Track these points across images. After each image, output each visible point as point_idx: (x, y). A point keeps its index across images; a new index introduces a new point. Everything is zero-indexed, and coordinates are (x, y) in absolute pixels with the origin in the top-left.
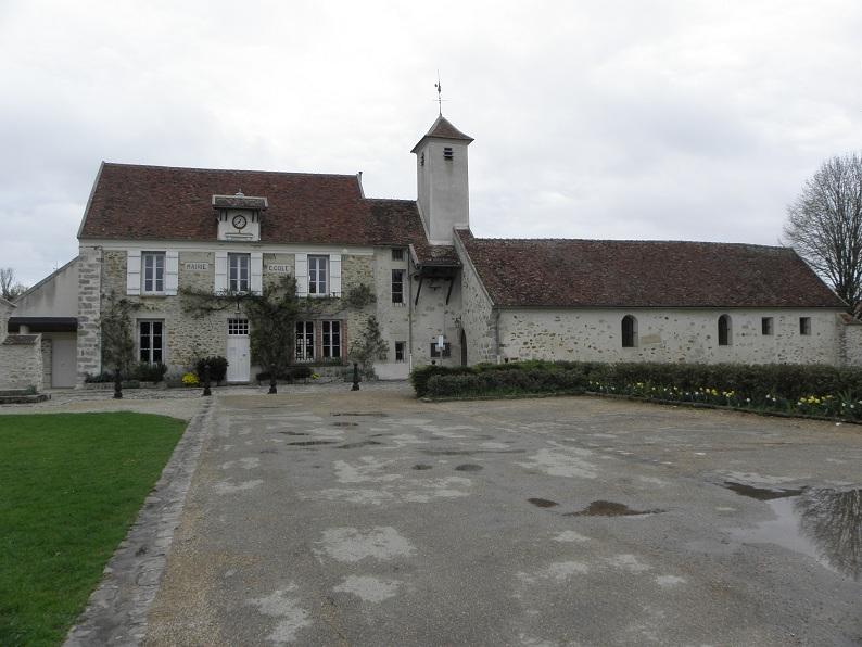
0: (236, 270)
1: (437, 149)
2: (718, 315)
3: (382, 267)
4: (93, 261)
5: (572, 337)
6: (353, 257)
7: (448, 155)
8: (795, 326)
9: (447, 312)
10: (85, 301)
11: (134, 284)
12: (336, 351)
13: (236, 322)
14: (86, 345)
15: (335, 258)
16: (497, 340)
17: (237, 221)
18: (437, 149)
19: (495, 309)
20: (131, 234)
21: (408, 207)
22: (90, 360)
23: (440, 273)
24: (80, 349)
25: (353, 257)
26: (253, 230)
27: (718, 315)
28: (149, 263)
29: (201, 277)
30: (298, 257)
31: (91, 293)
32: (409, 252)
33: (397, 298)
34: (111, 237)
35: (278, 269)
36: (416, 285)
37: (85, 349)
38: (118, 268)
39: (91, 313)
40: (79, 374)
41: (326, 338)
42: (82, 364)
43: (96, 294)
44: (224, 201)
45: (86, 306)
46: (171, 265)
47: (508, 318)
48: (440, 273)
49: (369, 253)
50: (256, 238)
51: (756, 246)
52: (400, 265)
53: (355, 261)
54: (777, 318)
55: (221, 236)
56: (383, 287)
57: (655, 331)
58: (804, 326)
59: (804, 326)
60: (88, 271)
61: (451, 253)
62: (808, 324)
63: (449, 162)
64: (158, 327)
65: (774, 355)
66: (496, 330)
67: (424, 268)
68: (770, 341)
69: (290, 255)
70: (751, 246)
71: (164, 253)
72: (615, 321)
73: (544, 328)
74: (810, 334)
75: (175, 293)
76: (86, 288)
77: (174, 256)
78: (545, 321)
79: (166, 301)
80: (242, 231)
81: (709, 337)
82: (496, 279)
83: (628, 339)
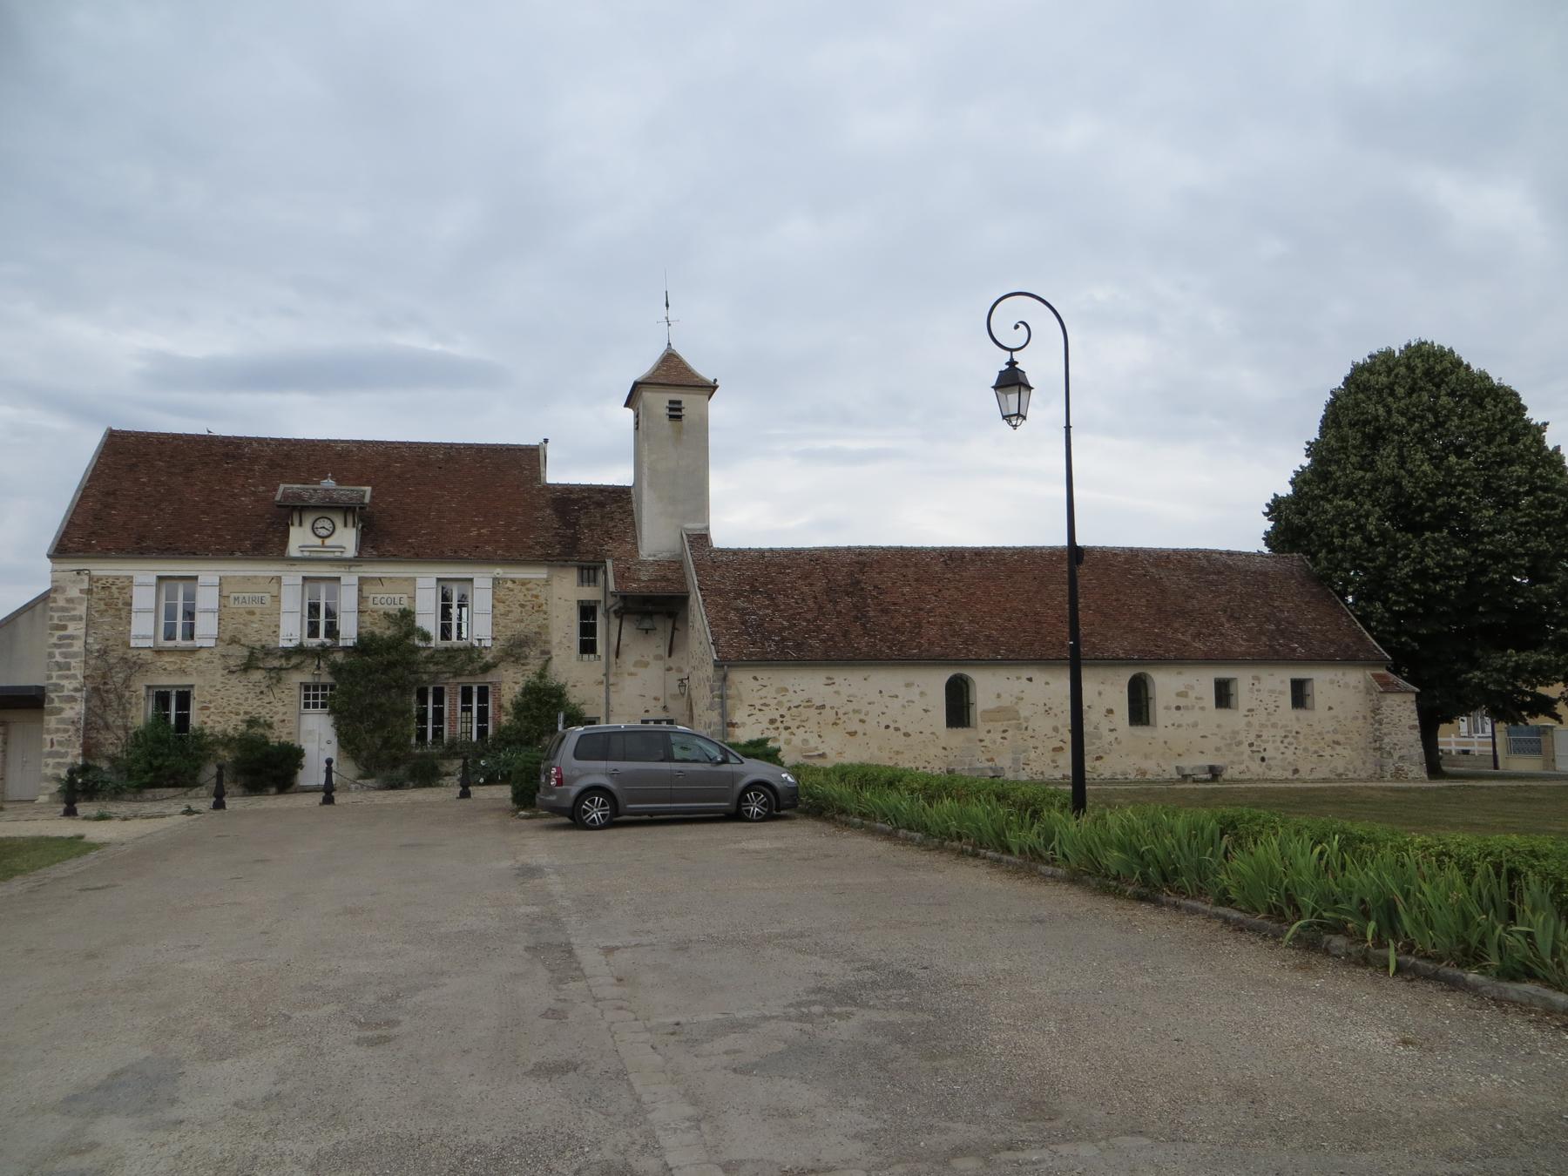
0: (175, 606)
1: (658, 401)
2: (1124, 676)
3: (564, 592)
4: (74, 592)
5: (855, 711)
6: (514, 581)
7: (675, 412)
8: (1281, 693)
9: (669, 669)
10: (58, 658)
11: (143, 628)
12: (438, 733)
13: (316, 688)
14: (57, 730)
15: (482, 582)
16: (723, 715)
17: (319, 524)
18: (658, 401)
19: (718, 665)
20: (141, 547)
21: (619, 496)
22: (65, 755)
23: (655, 607)
24: (48, 737)
25: (514, 581)
26: (346, 538)
27: (1124, 676)
28: (171, 596)
29: (256, 618)
30: (420, 583)
31: (71, 645)
32: (605, 573)
33: (588, 647)
34: (105, 554)
35: (387, 600)
36: (615, 622)
37: (56, 737)
38: (115, 603)
39: (67, 677)
40: (47, 779)
41: (422, 718)
42: (51, 761)
43: (78, 646)
44: (299, 496)
45: (60, 666)
46: (207, 599)
47: (743, 681)
48: (655, 607)
49: (538, 574)
50: (351, 552)
51: (1229, 554)
52: (590, 593)
53: (517, 588)
54: (1244, 679)
55: (293, 549)
56: (564, 628)
57: (1006, 701)
58: (1300, 694)
59: (1300, 694)
60: (63, 609)
61: (676, 564)
62: (1308, 690)
63: (676, 423)
64: (184, 699)
65: (1239, 743)
66: (722, 700)
67: (624, 598)
68: (1231, 720)
69: (407, 579)
70: (1221, 553)
71: (196, 578)
72: (933, 684)
73: (805, 696)
74: (1237, 708)
75: (212, 643)
76: (60, 638)
77: (210, 580)
78: (808, 684)
79: (197, 655)
80: (328, 542)
81: (1110, 711)
82: (732, 616)
83: (958, 709)
